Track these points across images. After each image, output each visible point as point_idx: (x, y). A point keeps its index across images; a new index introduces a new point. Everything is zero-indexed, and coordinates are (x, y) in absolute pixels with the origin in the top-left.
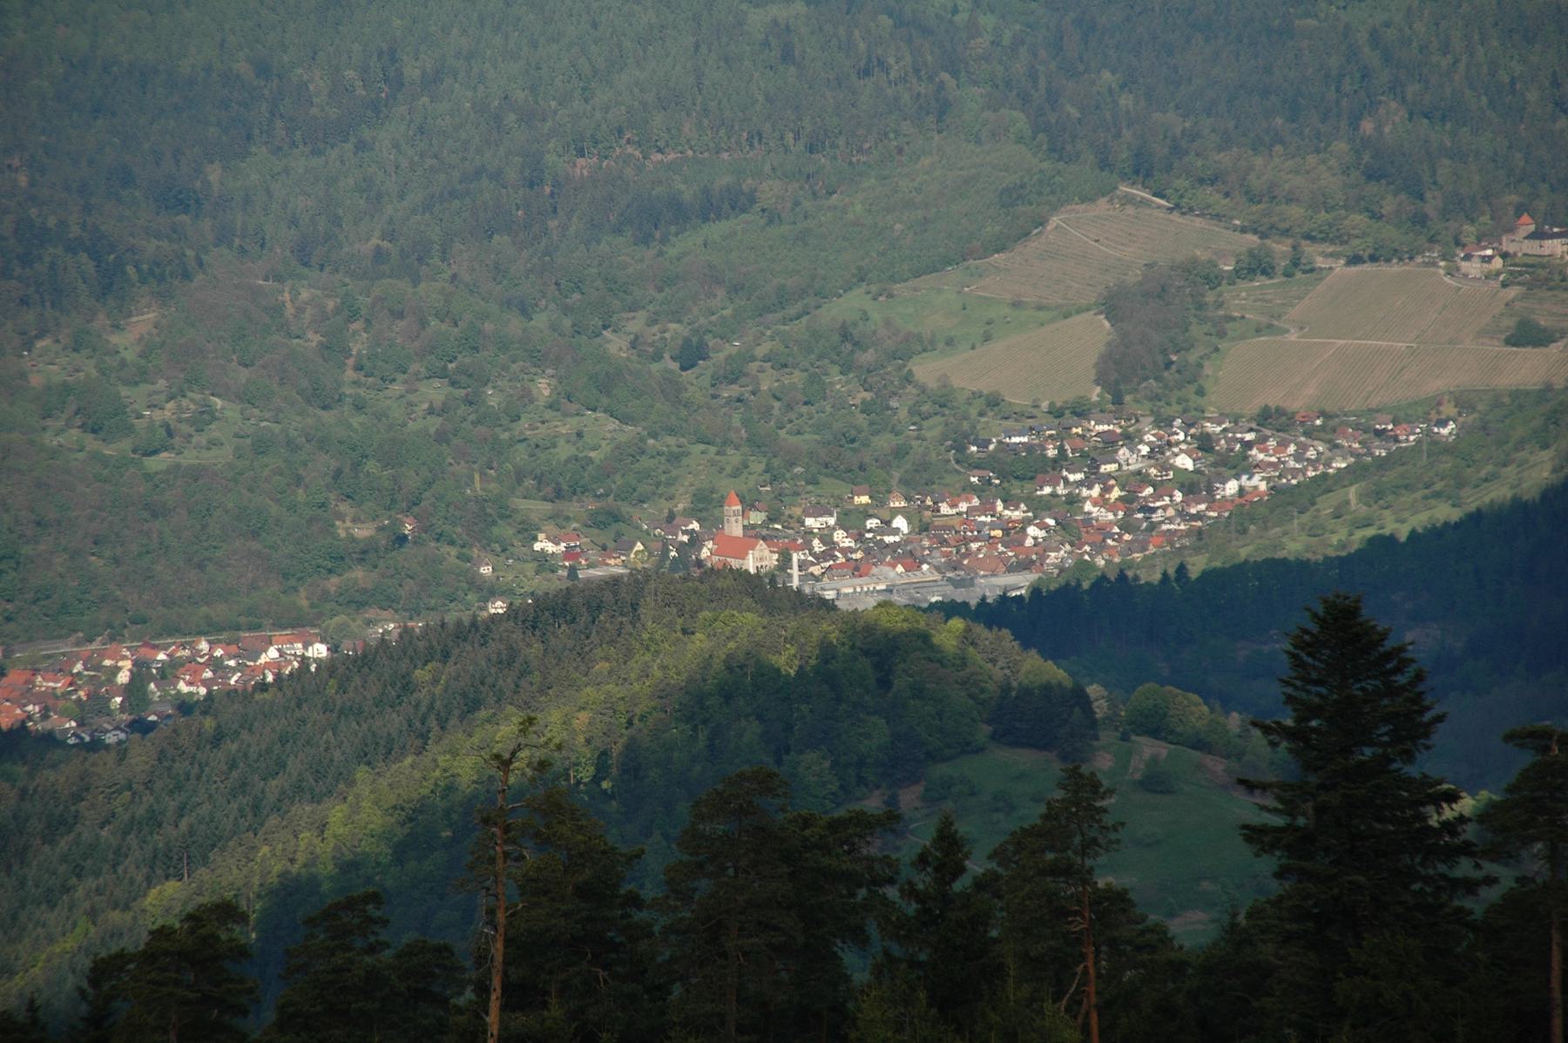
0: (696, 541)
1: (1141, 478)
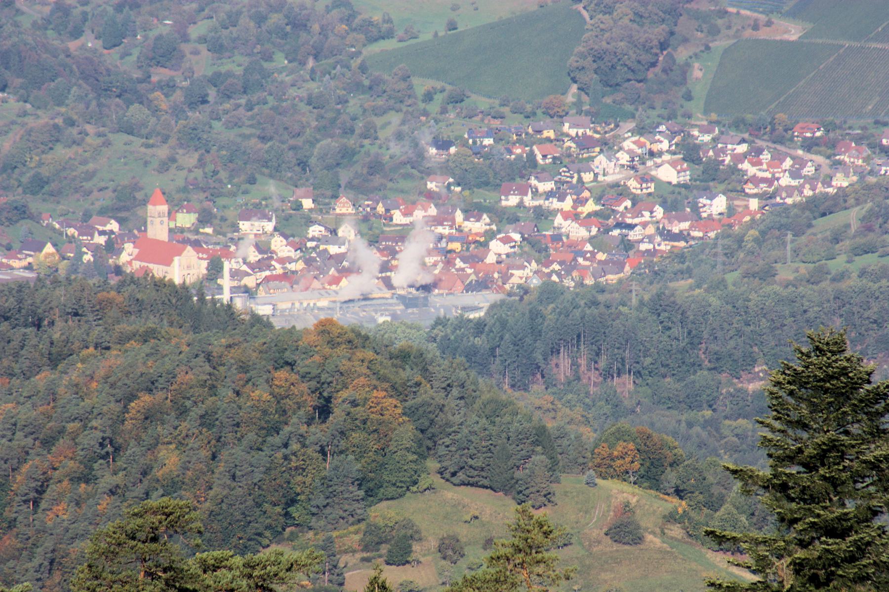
0: (113, 247)
1: (620, 191)
